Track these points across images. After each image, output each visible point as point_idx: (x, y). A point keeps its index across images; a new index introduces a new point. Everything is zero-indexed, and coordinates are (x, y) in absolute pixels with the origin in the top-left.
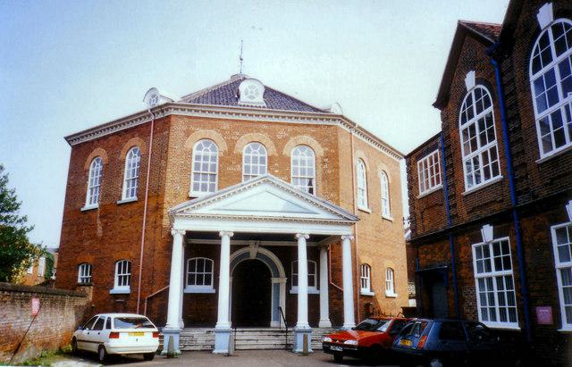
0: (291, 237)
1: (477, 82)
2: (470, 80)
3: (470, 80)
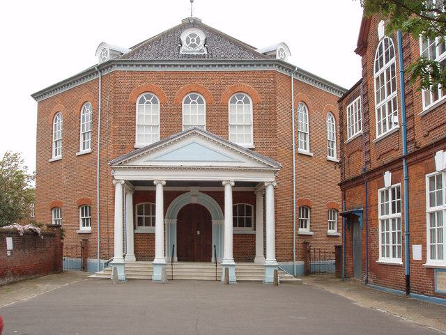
0: (219, 184)
2: (381, 28)
3: (381, 28)
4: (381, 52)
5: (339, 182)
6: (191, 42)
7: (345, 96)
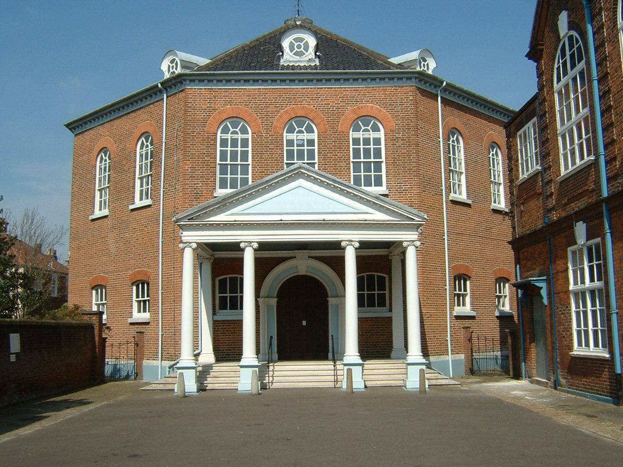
1: (570, 29)
4: (563, 55)
5: (510, 239)
6: (296, 49)
7: (514, 120)
